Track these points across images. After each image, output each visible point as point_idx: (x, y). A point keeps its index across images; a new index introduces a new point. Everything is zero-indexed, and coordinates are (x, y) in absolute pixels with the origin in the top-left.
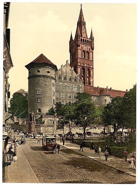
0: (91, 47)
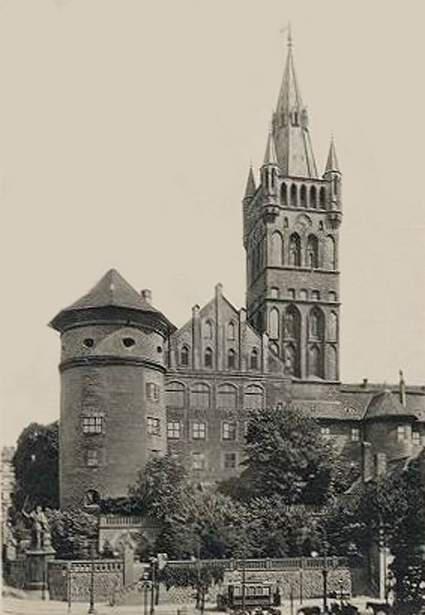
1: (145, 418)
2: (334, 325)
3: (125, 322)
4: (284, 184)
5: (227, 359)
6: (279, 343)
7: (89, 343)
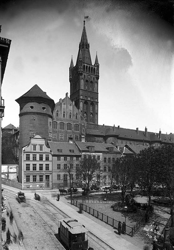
3: (43, 102)
4: (84, 65)
5: (56, 114)
6: (83, 112)
7: (32, 107)
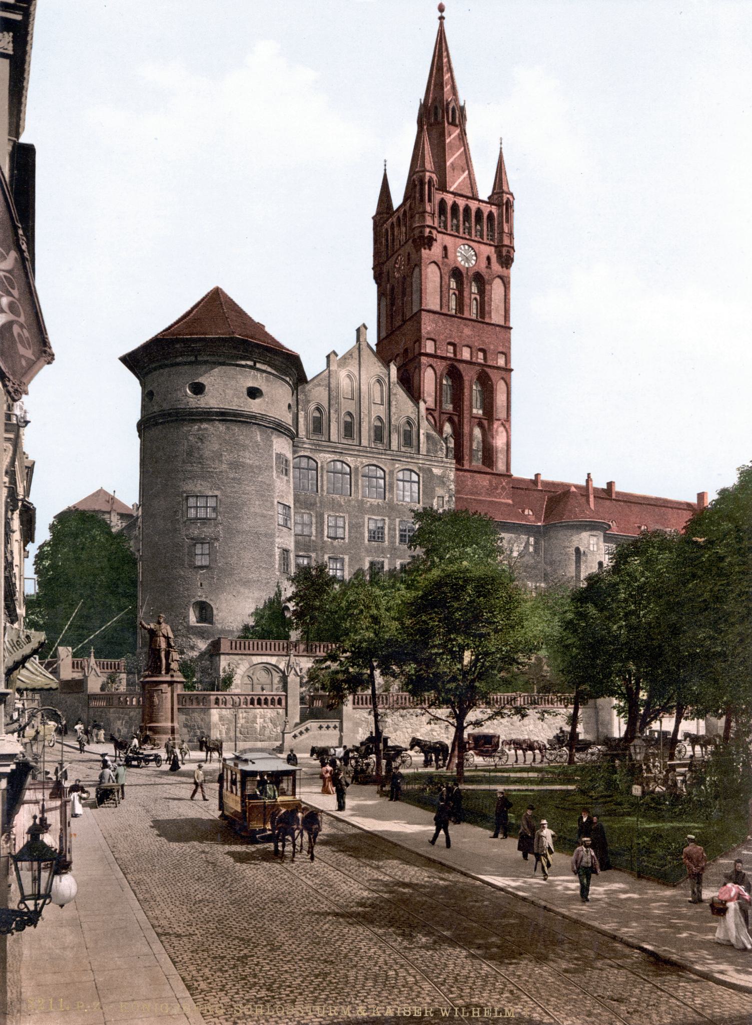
0: (499, 248)
1: (276, 503)
2: (504, 397)
